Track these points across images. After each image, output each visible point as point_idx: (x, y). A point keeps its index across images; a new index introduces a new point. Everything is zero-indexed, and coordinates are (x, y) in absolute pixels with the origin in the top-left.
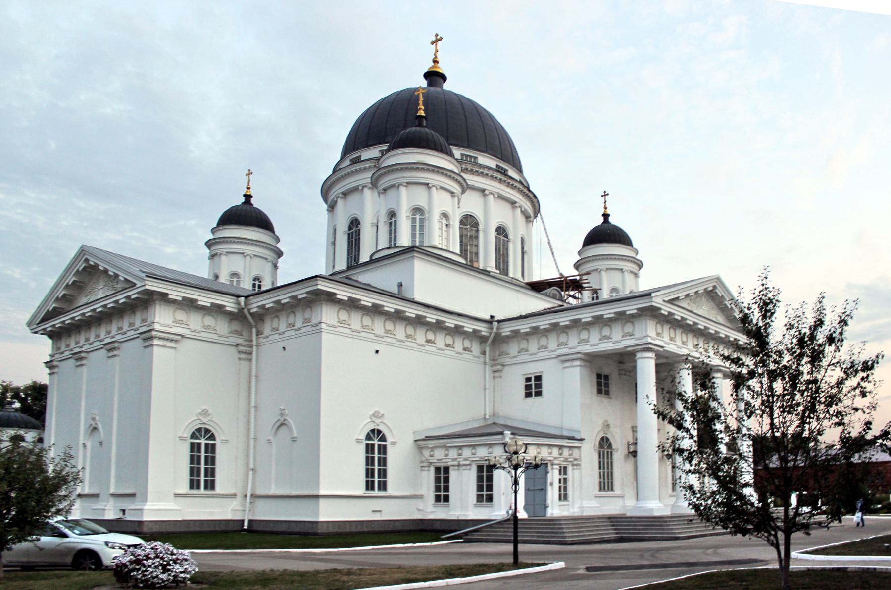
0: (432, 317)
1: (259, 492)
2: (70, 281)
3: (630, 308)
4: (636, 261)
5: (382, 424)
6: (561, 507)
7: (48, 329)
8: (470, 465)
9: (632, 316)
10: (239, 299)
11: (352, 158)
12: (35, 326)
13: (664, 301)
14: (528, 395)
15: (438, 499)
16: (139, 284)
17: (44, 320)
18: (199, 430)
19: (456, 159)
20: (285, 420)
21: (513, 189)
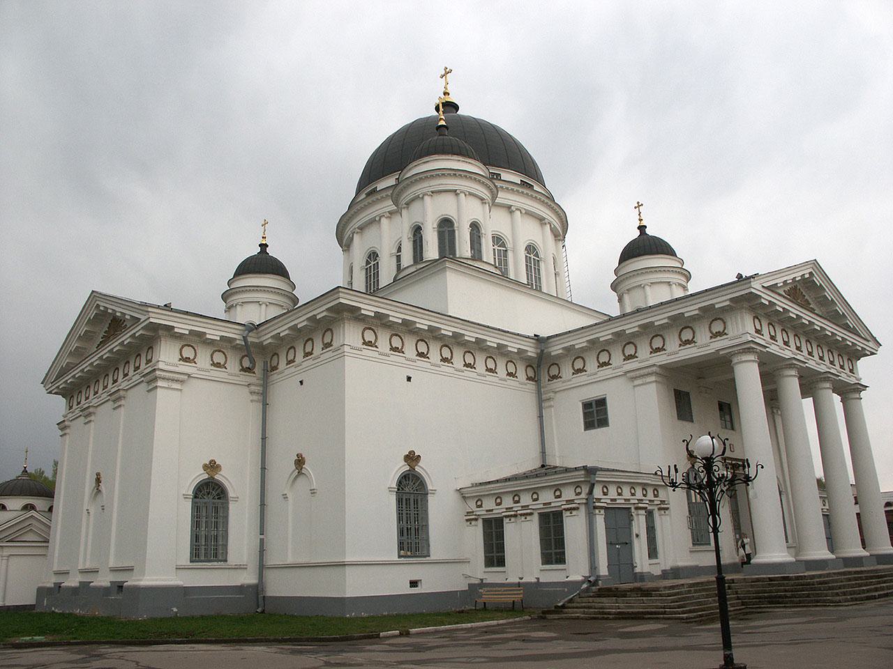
8: (531, 514)
12: (50, 386)
16: (143, 318)
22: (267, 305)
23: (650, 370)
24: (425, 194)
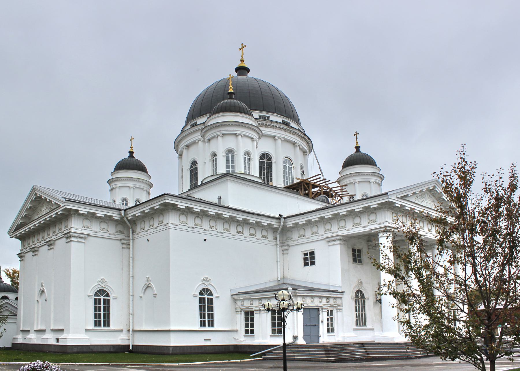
0: (240, 217)
1: (136, 328)
2: (28, 207)
3: (373, 204)
4: (379, 175)
5: (210, 285)
6: (329, 337)
7: (18, 235)
9: (375, 209)
10: (121, 211)
11: (191, 124)
12: (12, 234)
13: (397, 197)
14: (306, 264)
15: (247, 332)
17: (16, 230)
18: (99, 291)
19: (256, 119)
20: (149, 284)
21: (293, 134)
22: (134, 188)
23: (337, 238)
24: (218, 136)
